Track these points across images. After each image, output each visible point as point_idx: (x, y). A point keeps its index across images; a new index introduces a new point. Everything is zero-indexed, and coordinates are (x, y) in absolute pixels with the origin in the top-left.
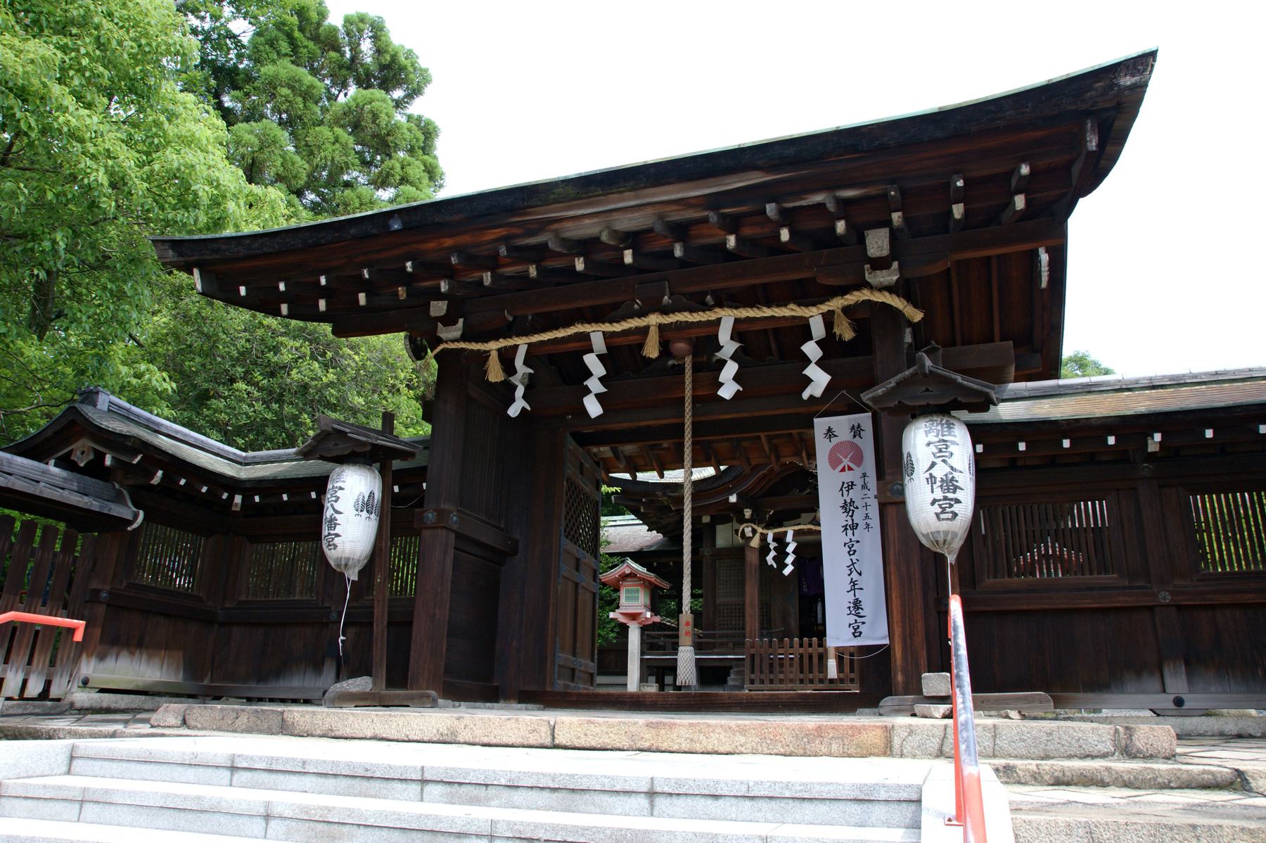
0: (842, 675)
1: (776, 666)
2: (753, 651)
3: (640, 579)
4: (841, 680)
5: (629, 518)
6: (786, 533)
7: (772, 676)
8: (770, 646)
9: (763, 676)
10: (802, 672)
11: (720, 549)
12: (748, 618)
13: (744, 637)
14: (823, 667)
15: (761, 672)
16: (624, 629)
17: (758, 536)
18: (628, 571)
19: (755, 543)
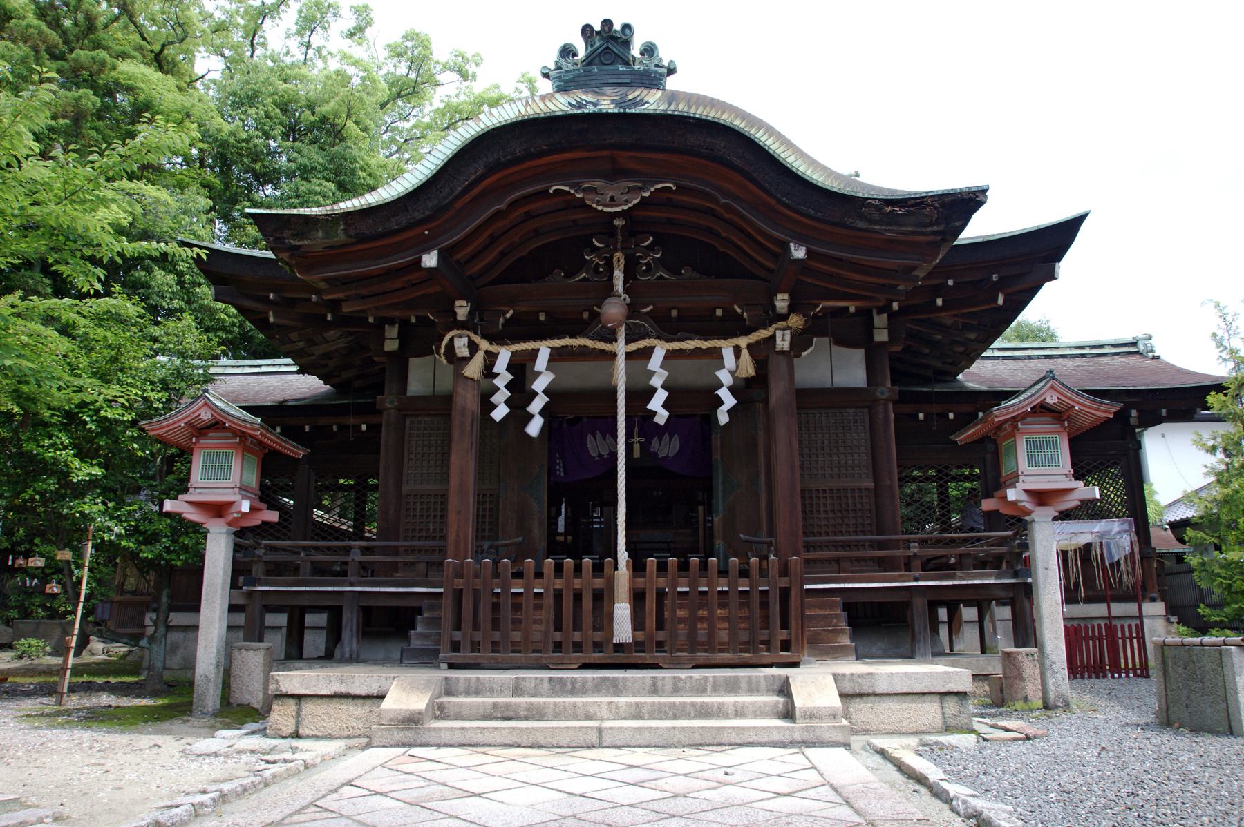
0: (640, 635)
1: (507, 613)
2: (459, 583)
3: (235, 433)
4: (638, 645)
5: (285, 364)
6: (535, 353)
7: (497, 635)
8: (496, 574)
9: (478, 636)
10: (558, 627)
11: (413, 398)
12: (452, 517)
13: (443, 552)
14: (604, 620)
15: (476, 627)
16: (199, 531)
17: (480, 356)
18: (206, 415)
19: (473, 369)
